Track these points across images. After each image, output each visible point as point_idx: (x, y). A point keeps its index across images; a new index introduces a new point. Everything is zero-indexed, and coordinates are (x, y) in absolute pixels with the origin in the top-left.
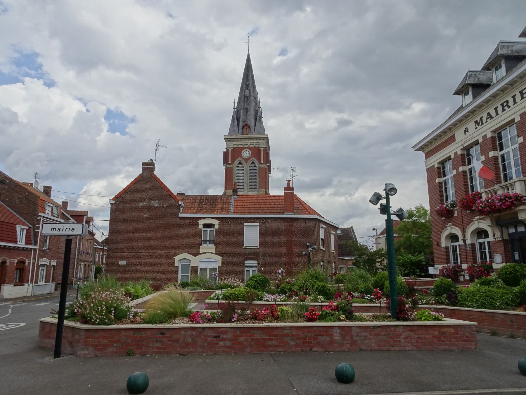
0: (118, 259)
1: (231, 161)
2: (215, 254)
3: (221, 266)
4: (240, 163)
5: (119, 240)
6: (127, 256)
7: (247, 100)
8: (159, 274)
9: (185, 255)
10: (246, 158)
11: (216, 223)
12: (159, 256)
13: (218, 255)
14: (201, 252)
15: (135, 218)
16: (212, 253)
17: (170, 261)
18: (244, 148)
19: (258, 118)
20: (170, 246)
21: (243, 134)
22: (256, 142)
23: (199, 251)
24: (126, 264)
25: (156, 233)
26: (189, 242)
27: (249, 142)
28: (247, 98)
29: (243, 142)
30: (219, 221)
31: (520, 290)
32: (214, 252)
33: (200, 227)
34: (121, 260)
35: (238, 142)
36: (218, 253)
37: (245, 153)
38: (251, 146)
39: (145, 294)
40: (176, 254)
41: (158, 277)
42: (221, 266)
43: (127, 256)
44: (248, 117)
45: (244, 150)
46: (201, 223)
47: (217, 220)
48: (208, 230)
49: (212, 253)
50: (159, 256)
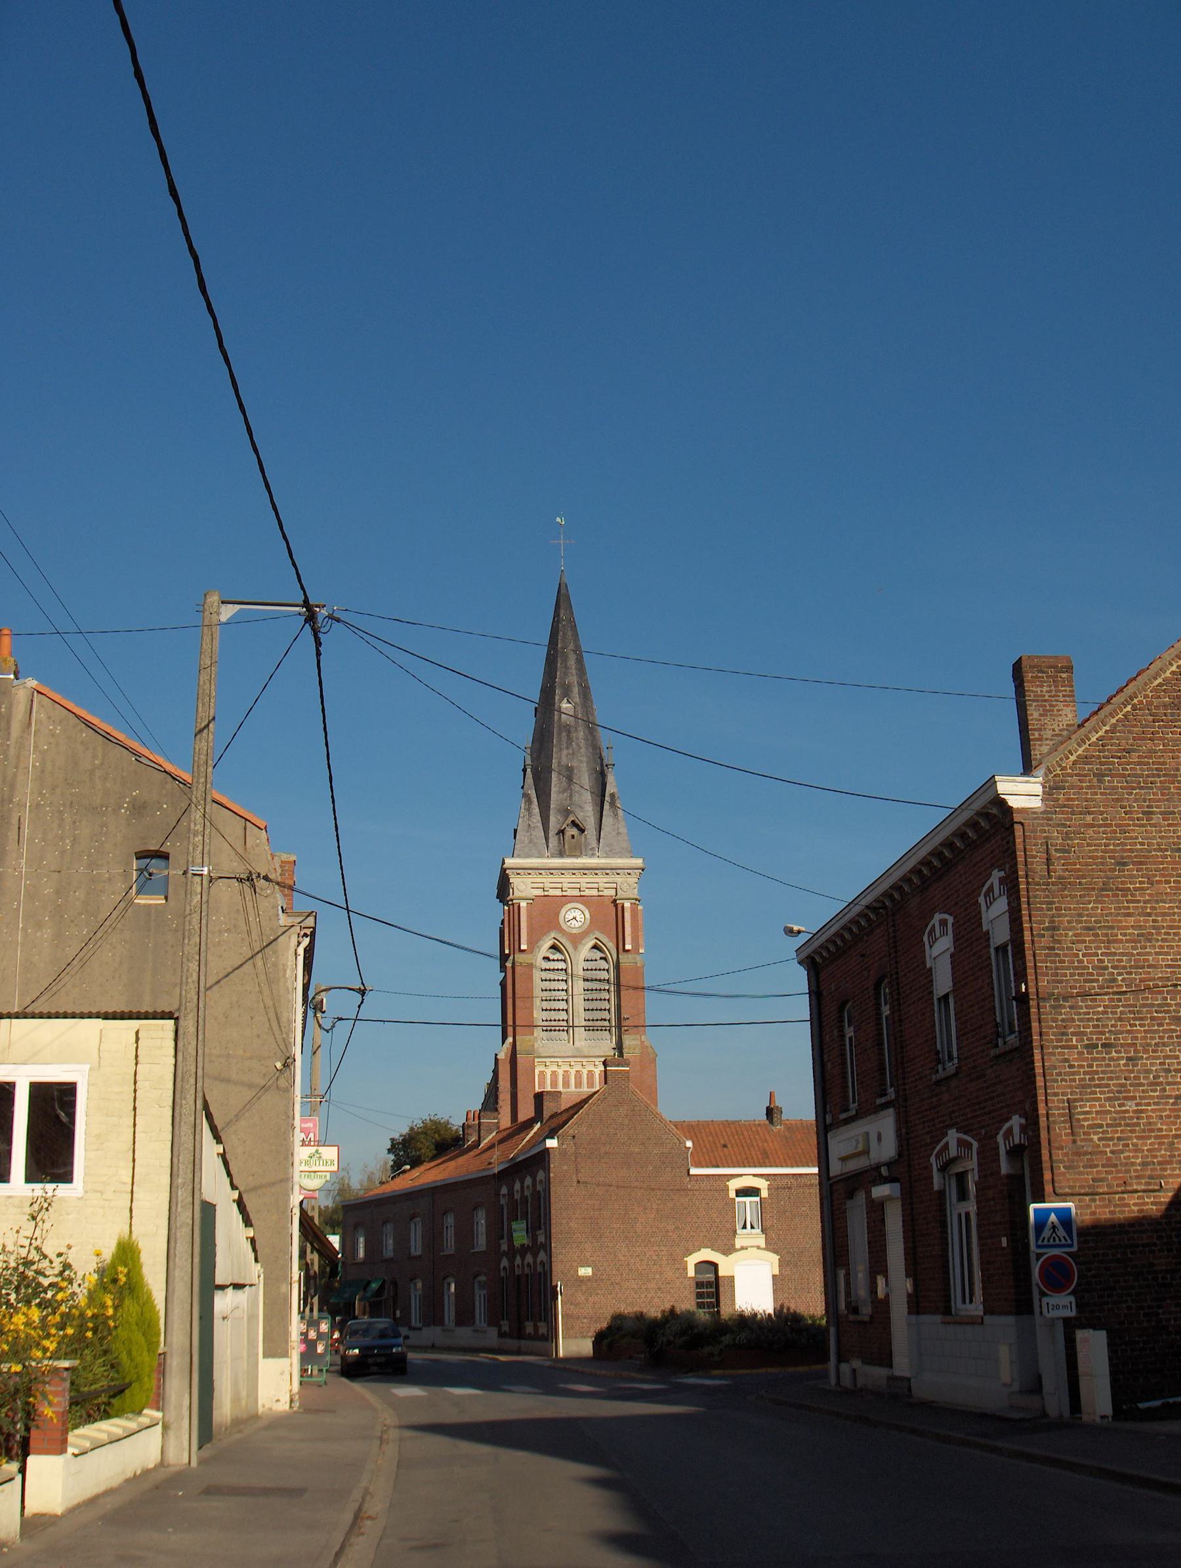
0: (575, 1264)
1: (529, 943)
2: (764, 1249)
3: (778, 1273)
4: (554, 947)
5: (573, 1225)
6: (592, 1259)
7: (569, 738)
8: (659, 1294)
9: (706, 1254)
10: (574, 931)
11: (762, 1184)
12: (655, 1257)
13: (770, 1251)
14: (738, 1246)
15: (601, 1179)
16: (758, 1248)
17: (677, 1266)
18: (573, 899)
19: (607, 798)
20: (675, 1236)
21: (561, 854)
22: (605, 880)
23: (734, 1245)
24: (591, 1274)
25: (645, 1209)
26: (711, 1227)
27: (583, 881)
28: (569, 732)
29: (566, 880)
30: (769, 1183)
31: (360, 1528)
32: (763, 1245)
33: (732, 1194)
34: (581, 1266)
35: (547, 880)
36: (771, 1246)
37: (570, 916)
38: (587, 892)
39: (63, 1357)
40: (689, 1253)
41: (656, 1300)
42: (778, 1273)
43: (592, 1259)
44: (576, 798)
45: (569, 906)
46: (734, 1185)
47: (764, 1181)
48: (747, 1200)
49: (758, 1248)
50: (655, 1257)
